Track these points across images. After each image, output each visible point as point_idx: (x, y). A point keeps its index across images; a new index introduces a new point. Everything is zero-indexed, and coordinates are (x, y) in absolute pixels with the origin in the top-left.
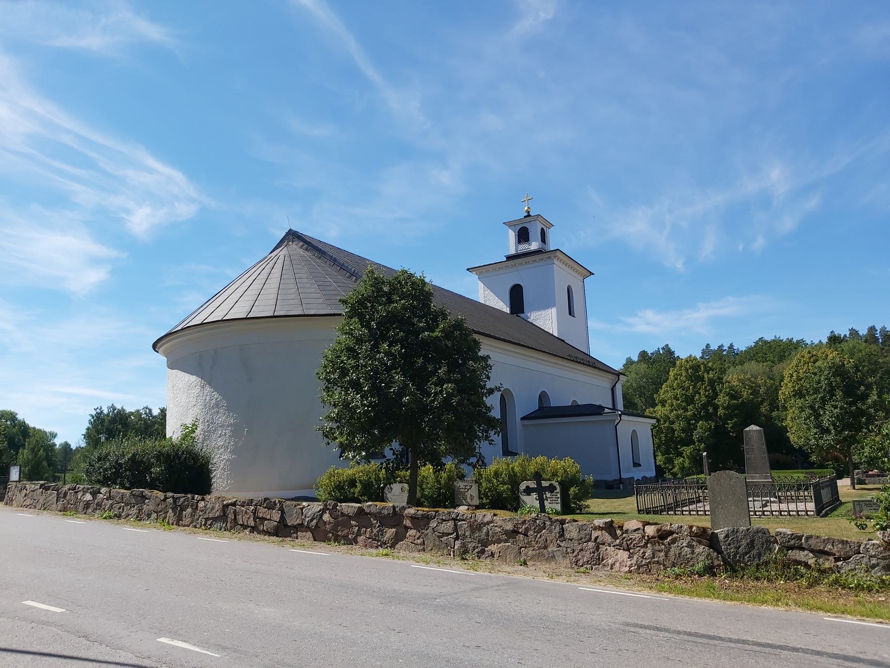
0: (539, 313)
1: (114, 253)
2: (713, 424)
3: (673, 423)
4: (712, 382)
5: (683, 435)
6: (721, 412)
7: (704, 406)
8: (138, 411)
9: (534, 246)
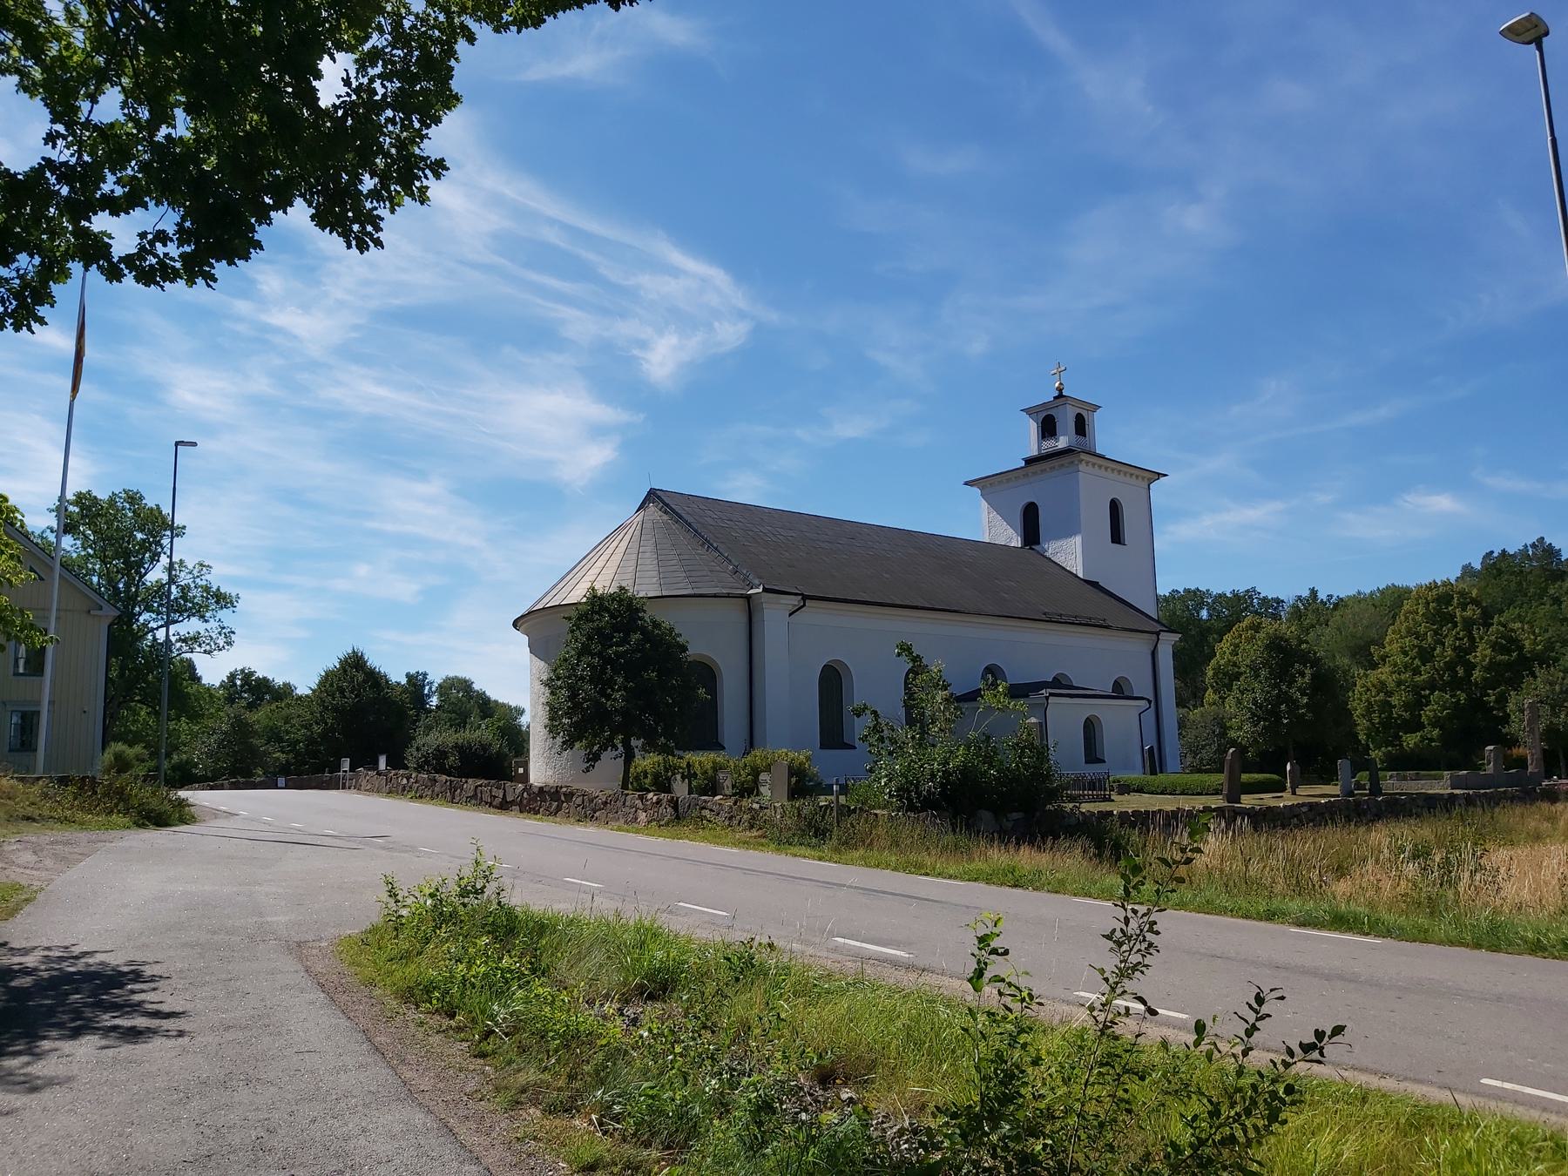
0: (1059, 543)
1: (623, 416)
2: (1463, 697)
3: (1389, 694)
4: (1468, 624)
5: (1406, 715)
6: (1477, 674)
7: (1450, 666)
8: (1279, 601)
9: (1062, 442)
